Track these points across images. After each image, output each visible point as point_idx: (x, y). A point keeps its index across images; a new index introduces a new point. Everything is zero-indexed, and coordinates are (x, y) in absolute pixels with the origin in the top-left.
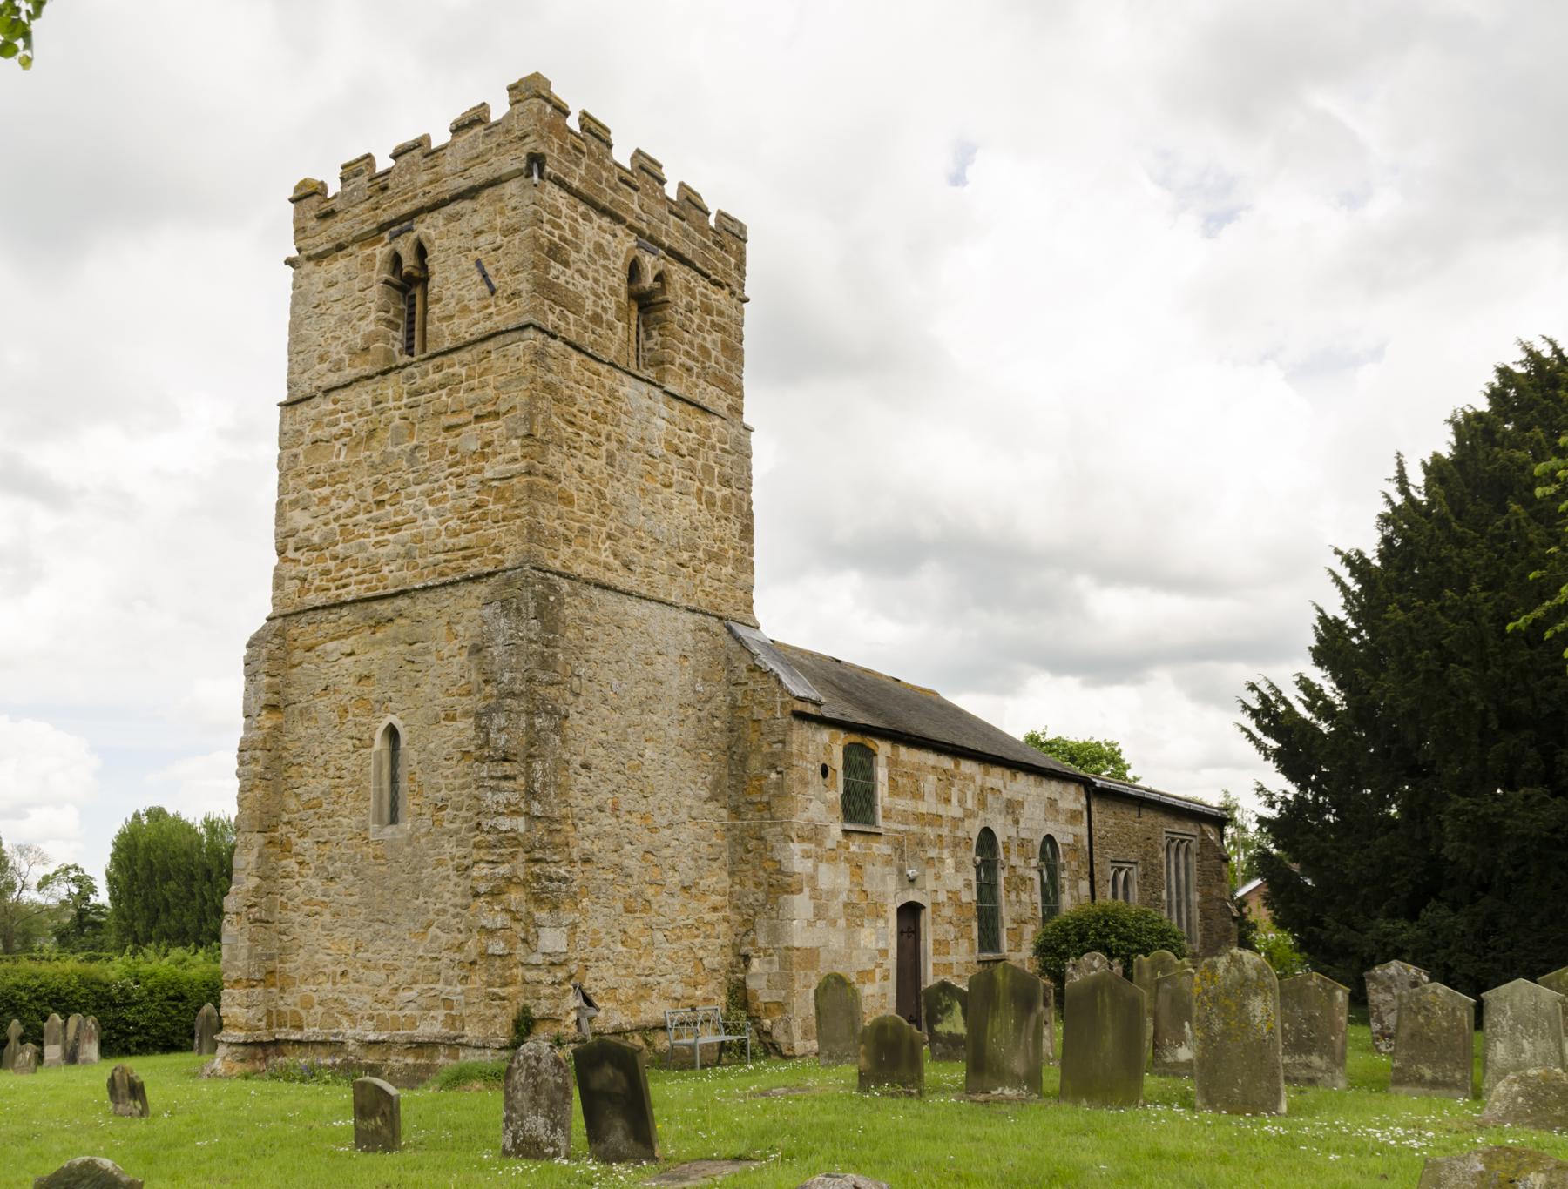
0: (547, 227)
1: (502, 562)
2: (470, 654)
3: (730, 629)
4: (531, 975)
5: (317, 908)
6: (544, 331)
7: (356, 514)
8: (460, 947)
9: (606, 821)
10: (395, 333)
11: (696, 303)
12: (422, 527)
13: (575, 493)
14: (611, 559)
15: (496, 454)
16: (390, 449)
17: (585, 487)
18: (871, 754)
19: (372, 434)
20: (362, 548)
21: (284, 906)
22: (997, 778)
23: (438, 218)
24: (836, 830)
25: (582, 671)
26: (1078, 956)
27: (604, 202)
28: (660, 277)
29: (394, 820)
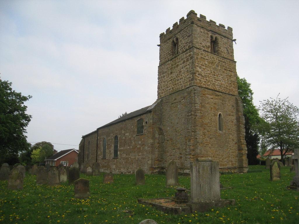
23: (145, 115)
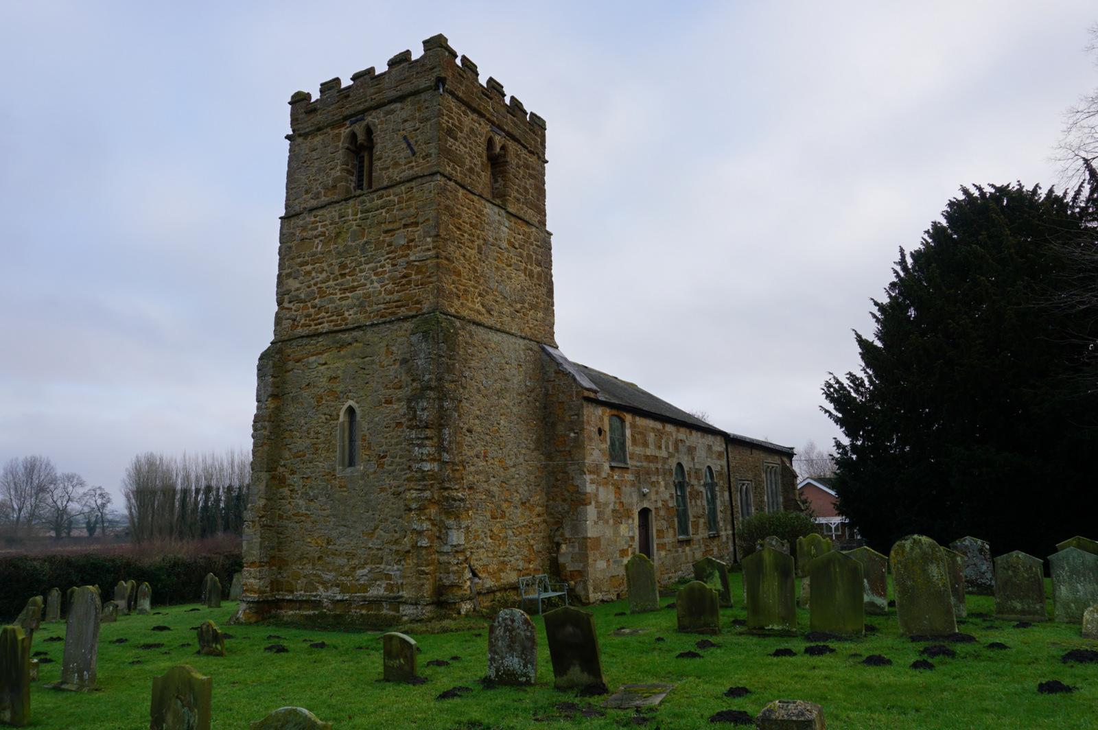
0: (446, 118)
1: (421, 309)
2: (401, 364)
3: (543, 349)
4: (444, 558)
5: (303, 518)
6: (445, 176)
7: (328, 281)
8: (396, 542)
9: (481, 464)
10: (351, 177)
11: (521, 163)
12: (370, 288)
13: (461, 269)
14: (481, 308)
15: (416, 246)
16: (350, 243)
17: (467, 266)
18: (623, 421)
19: (338, 235)
20: (332, 301)
21: (281, 517)
22: (682, 434)
23: (380, 113)
24: (606, 466)
25: (467, 374)
26: (763, 539)
27: (474, 105)
28: (503, 148)
29: (352, 463)
